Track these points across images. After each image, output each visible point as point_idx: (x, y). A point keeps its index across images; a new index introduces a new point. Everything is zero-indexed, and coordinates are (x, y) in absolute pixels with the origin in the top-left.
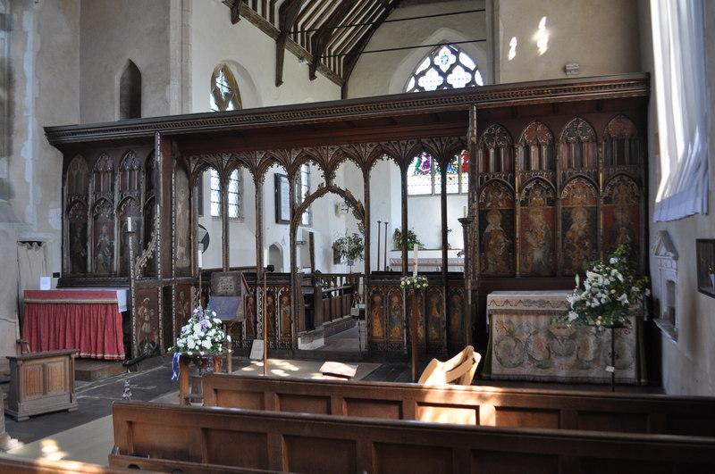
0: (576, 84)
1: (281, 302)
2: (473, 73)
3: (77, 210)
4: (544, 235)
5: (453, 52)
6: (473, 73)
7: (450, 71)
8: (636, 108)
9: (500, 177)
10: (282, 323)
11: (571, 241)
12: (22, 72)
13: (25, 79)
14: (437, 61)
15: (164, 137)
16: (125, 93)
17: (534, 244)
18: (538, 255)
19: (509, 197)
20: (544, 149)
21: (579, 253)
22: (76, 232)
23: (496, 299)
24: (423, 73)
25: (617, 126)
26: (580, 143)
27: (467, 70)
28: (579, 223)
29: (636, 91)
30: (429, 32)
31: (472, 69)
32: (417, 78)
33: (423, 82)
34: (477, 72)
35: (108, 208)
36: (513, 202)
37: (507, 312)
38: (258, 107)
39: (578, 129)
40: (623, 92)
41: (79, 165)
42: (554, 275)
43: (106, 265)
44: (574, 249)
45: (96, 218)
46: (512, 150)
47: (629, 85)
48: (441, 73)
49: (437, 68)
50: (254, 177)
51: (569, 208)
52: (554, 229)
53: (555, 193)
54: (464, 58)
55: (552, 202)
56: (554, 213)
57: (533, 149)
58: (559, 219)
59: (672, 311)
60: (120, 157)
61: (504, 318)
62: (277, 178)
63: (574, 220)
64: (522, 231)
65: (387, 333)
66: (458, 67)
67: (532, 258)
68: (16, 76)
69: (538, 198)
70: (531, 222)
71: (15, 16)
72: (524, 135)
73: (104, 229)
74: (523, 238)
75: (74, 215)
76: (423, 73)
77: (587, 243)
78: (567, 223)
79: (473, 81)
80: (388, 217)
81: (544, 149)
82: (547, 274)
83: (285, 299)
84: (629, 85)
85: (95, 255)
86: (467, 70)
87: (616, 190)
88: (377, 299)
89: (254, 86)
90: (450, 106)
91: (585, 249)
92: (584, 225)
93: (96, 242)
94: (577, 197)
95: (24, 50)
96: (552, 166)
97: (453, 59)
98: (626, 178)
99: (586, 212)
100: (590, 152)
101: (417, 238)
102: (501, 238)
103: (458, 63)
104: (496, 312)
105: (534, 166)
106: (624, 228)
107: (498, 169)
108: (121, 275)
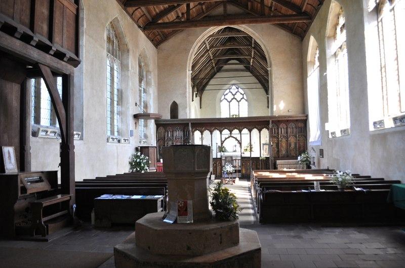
2: (243, 95)
6: (243, 95)
7: (235, 94)
8: (305, 122)
12: (150, 104)
13: (150, 106)
18: (284, 152)
23: (278, 162)
24: (227, 94)
26: (293, 128)
27: (241, 94)
28: (293, 146)
29: (305, 118)
30: (230, 81)
32: (225, 95)
36: (278, 141)
37: (281, 164)
38: (215, 117)
40: (302, 118)
42: (288, 156)
46: (278, 129)
48: (233, 95)
49: (231, 92)
52: (287, 147)
54: (240, 90)
55: (287, 141)
56: (287, 143)
57: (283, 129)
58: (288, 145)
59: (314, 163)
61: (280, 165)
65: (246, 172)
66: (238, 93)
68: (148, 105)
69: (284, 140)
71: (148, 89)
72: (281, 126)
74: (281, 149)
76: (227, 94)
78: (290, 146)
80: (245, 143)
86: (241, 94)
88: (244, 164)
90: (265, 120)
94: (292, 140)
95: (150, 99)
96: (287, 133)
100: (295, 130)
101: (130, 160)
102: (276, 149)
103: (238, 91)
104: (279, 164)
105: (283, 133)
107: (275, 133)
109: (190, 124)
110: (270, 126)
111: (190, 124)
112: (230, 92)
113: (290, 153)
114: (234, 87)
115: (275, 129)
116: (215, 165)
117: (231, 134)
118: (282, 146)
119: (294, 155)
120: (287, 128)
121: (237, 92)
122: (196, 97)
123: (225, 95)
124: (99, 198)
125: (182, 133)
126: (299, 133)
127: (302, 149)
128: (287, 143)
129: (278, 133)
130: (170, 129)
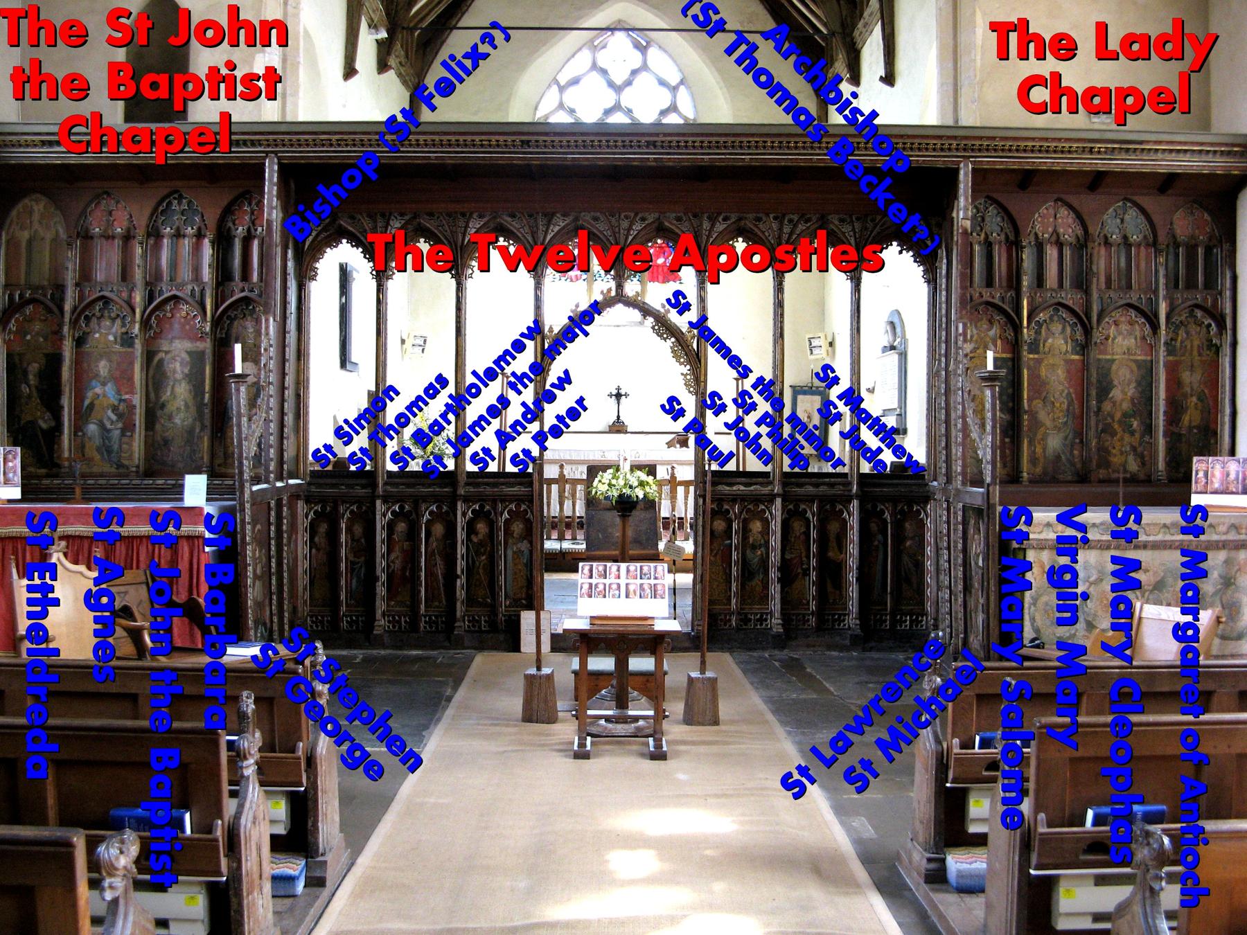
0: (1148, 142)
1: (508, 533)
3: (29, 320)
4: (1065, 406)
5: (637, 46)
6: (674, 89)
9: (45, 296)
10: (509, 578)
11: (1109, 420)
14: (603, 59)
15: (286, 171)
16: (722, 84)
17: (1048, 423)
18: (1054, 442)
19: (1010, 334)
20: (1067, 252)
21: (1122, 439)
22: (25, 373)
24: (575, 81)
25: (1184, 223)
27: (662, 83)
31: (673, 83)
32: (562, 89)
33: (572, 97)
34: (682, 88)
35: (113, 320)
39: (1120, 221)
41: (36, 217)
43: (109, 451)
44: (1113, 434)
45: (80, 342)
46: (1014, 244)
47: (1229, 153)
50: (375, 268)
51: (1108, 360)
52: (1083, 397)
53: (1087, 332)
57: (1051, 253)
58: (1091, 382)
60: (152, 203)
62: (345, 275)
63: (1116, 382)
64: (1030, 400)
67: (1044, 449)
70: (1044, 384)
73: (103, 367)
74: (1033, 415)
75: (21, 332)
76: (575, 81)
77: (1135, 424)
78: (1104, 390)
79: (673, 108)
81: (1067, 252)
82: (1069, 478)
83: (518, 527)
84: (1229, 153)
85: (78, 428)
86: (662, 83)
87: (1182, 334)
89: (318, 74)
91: (1132, 433)
92: (1131, 391)
93: (79, 395)
96: (1082, 283)
97: (636, 59)
98: (1199, 313)
99: (1135, 368)
103: (645, 67)
106: (1194, 399)
107: (989, 283)
108: (149, 473)
109: (271, 173)
110: (963, 212)
111: (271, 173)
112: (594, 66)
113: (1103, 451)
114: (620, 40)
115: (988, 245)
116: (481, 527)
117: (620, 287)
118: (1039, 387)
119: (1133, 466)
120: (1082, 245)
121: (634, 72)
122: (382, 67)
123: (562, 89)
124: (14, 571)
125: (207, 251)
126: (1173, 283)
127: (1191, 417)
128: (1085, 366)
129: (1014, 281)
130: (126, 213)
